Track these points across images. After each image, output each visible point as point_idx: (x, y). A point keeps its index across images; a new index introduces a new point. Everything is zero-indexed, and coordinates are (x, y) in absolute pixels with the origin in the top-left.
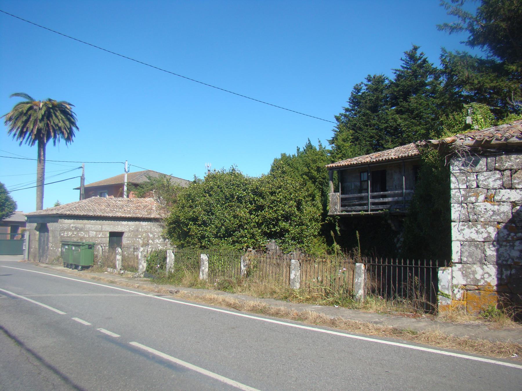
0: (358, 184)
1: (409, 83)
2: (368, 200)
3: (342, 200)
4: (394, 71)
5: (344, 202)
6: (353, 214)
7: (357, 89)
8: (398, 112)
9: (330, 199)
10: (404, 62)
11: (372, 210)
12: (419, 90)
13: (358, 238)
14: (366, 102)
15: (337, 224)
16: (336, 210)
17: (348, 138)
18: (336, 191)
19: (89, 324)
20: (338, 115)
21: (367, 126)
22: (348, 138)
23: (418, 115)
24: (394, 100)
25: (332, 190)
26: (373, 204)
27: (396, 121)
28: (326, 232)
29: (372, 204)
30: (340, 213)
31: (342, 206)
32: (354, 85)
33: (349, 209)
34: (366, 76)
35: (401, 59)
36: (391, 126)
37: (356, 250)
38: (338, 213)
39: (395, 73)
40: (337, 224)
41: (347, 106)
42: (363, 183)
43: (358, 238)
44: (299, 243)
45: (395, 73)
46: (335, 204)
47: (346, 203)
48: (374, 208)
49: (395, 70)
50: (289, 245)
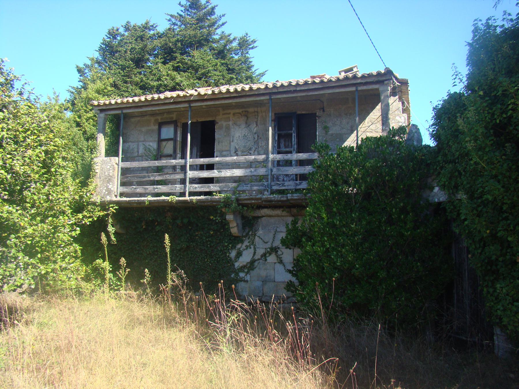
0: (154, 145)
1: (192, 33)
2: (185, 173)
3: (125, 172)
4: (169, 17)
5: (127, 177)
6: (150, 202)
7: (113, 34)
8: (176, 69)
9: (97, 168)
10: (183, 9)
11: (191, 194)
12: (204, 45)
13: (168, 250)
14: (126, 52)
15: (110, 220)
16: (109, 192)
17: (105, 88)
18: (112, 151)
19: (270, 128)
20: (81, 66)
21: (126, 82)
22: (105, 88)
23: (204, 75)
24: (167, 55)
25: (103, 151)
26: (193, 181)
27: (173, 79)
28: (89, 238)
29: (184, 181)
30: (119, 199)
31: (123, 184)
32: (111, 28)
33: (140, 190)
34: (124, 24)
35: (180, 4)
36: (165, 85)
37: (174, 282)
38: (114, 199)
39: (169, 20)
40: (110, 220)
41: (97, 55)
42: (164, 143)
43: (168, 250)
44: (42, 261)
45: (169, 20)
46: (109, 180)
47: (130, 177)
48: (198, 190)
49: (171, 16)
50: (17, 266)
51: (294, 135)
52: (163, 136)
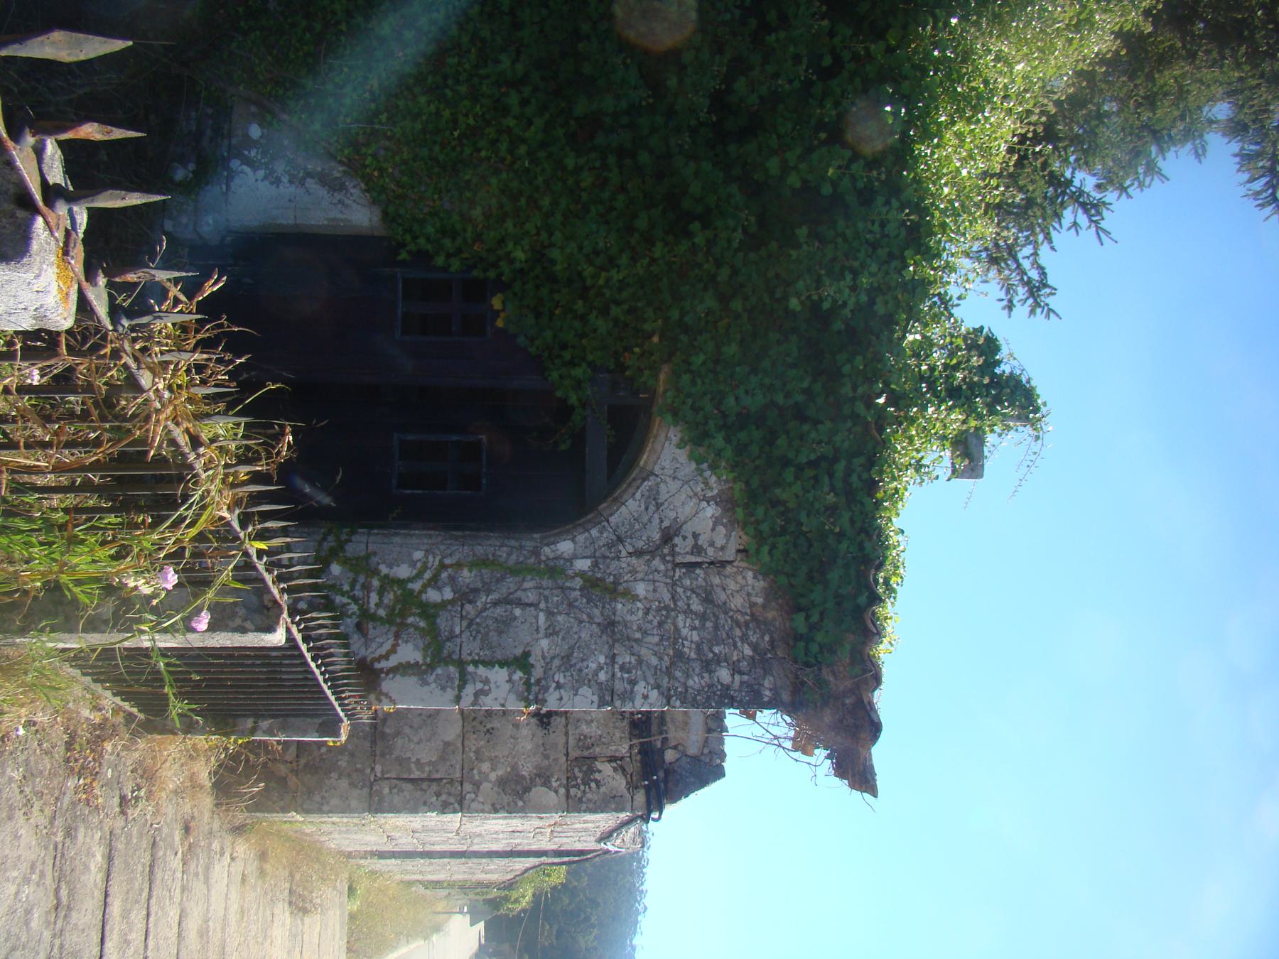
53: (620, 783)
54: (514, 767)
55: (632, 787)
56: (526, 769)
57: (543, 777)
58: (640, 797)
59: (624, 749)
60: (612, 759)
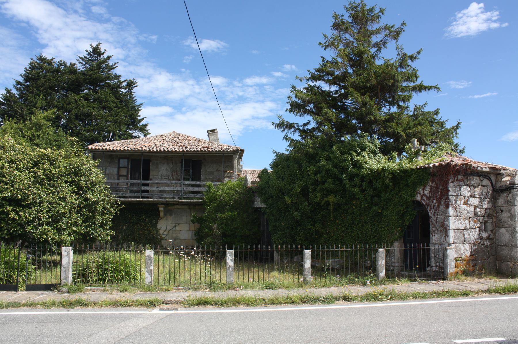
42: (121, 169)
51: (191, 171)
52: (121, 165)
53: (511, 195)
54: (509, 217)
55: (511, 192)
56: (509, 215)
57: (510, 211)
58: (512, 191)
59: (505, 194)
60: (507, 197)
